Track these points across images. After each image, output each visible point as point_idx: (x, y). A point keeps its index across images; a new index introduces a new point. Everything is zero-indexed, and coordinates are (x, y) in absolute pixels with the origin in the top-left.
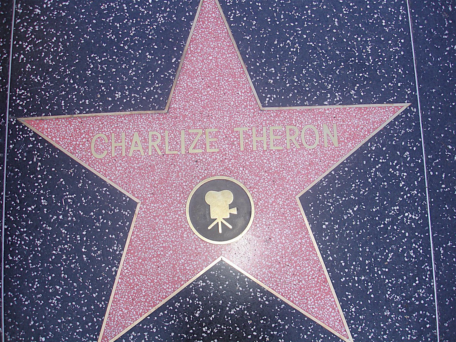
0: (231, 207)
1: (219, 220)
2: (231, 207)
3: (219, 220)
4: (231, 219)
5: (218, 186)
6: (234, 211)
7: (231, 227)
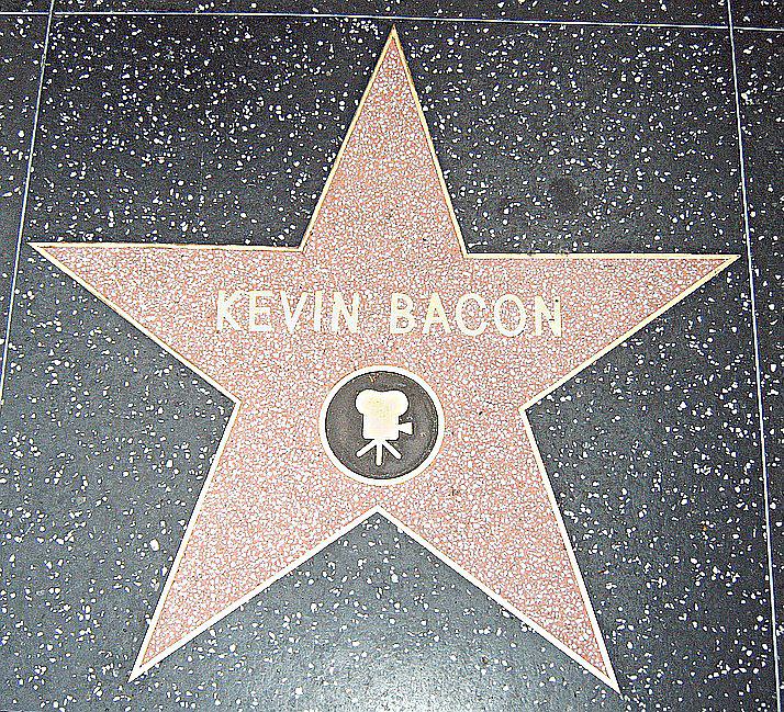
1: (379, 442)
2: (402, 420)
3: (379, 442)
5: (383, 382)
6: (407, 428)
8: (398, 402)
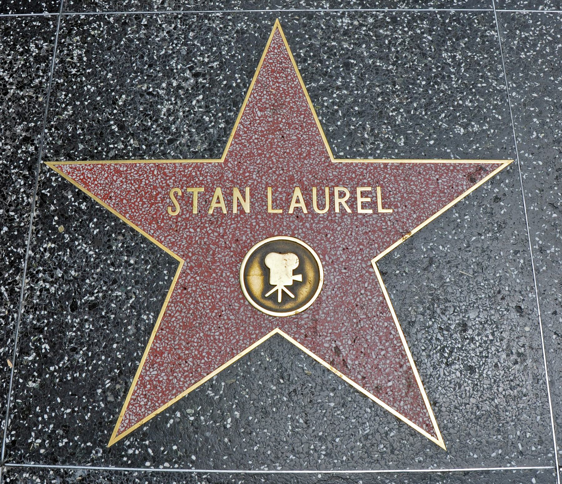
0: (295, 272)
1: (280, 287)
2: (295, 272)
3: (280, 287)
4: (295, 287)
6: (299, 278)
7: (280, 300)
8: (293, 261)
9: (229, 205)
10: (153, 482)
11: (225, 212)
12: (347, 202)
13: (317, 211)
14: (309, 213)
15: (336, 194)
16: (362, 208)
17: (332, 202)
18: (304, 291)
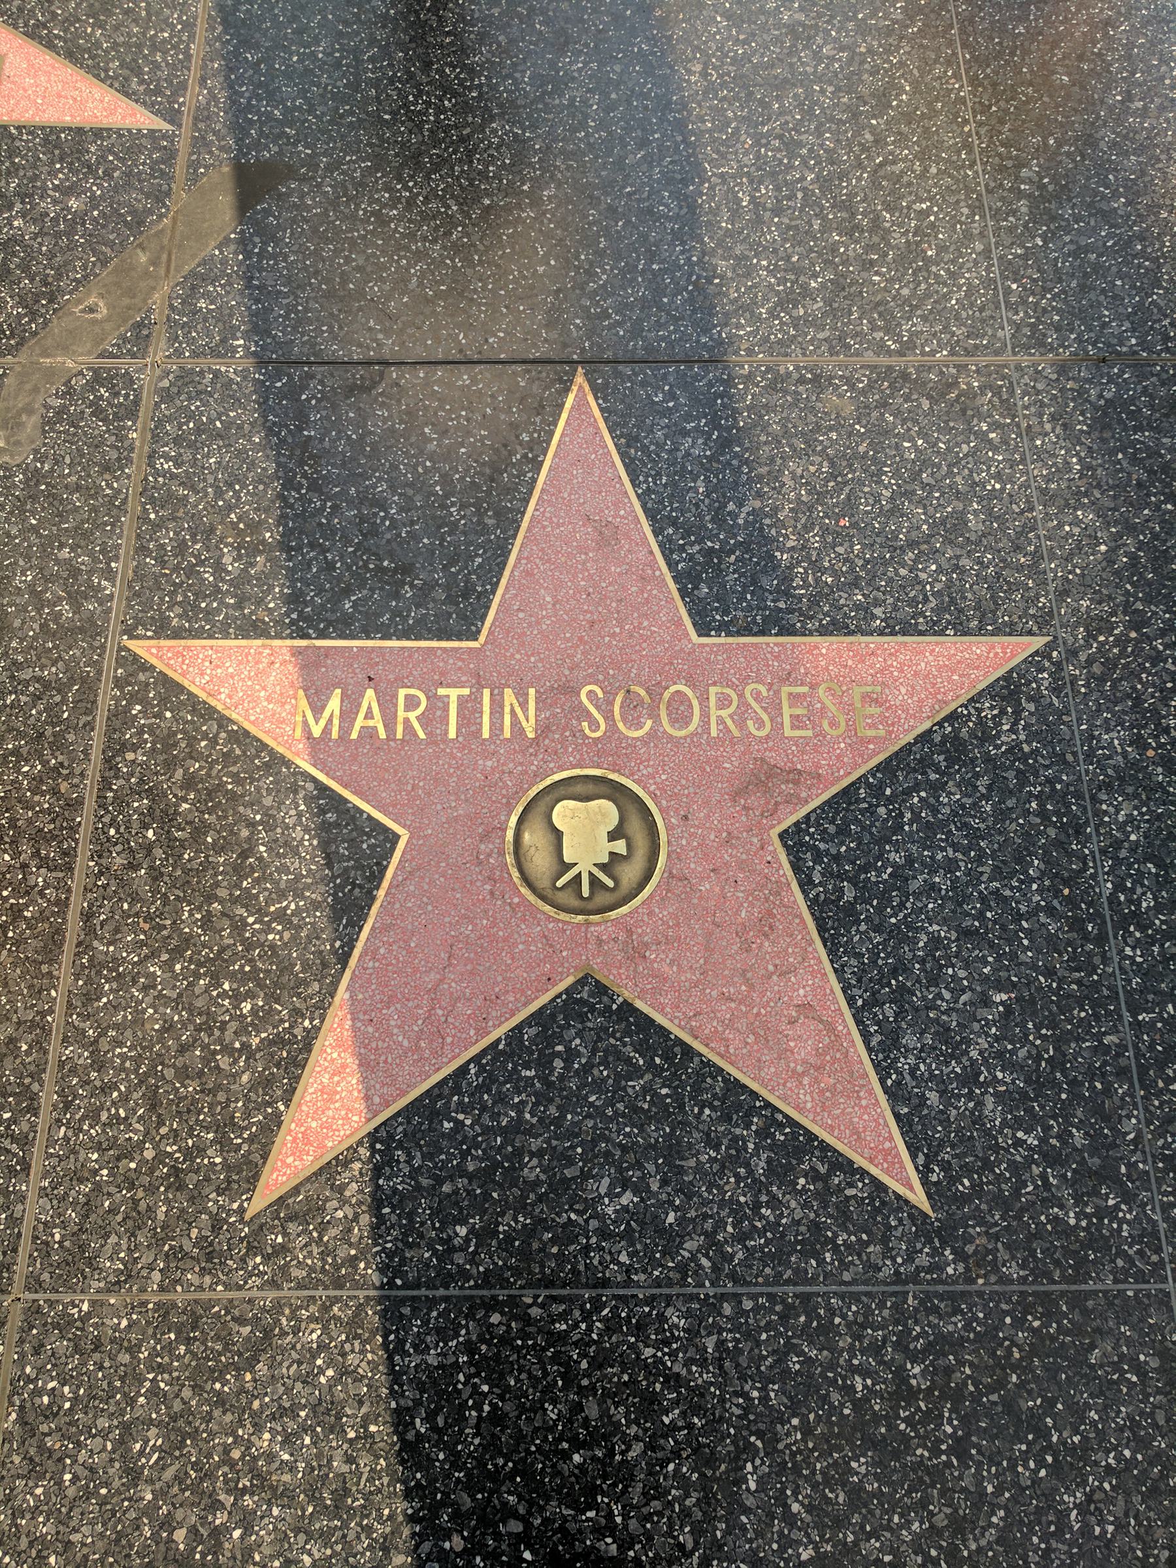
0: (613, 836)
1: (584, 867)
2: (613, 836)
3: (584, 867)
6: (620, 846)
8: (607, 811)
9: (390, 725)
10: (1174, 950)
11: (382, 734)
12: (731, 716)
13: (594, 735)
14: (388, 739)
15: (713, 700)
16: (793, 727)
17: (705, 715)
18: (630, 873)
